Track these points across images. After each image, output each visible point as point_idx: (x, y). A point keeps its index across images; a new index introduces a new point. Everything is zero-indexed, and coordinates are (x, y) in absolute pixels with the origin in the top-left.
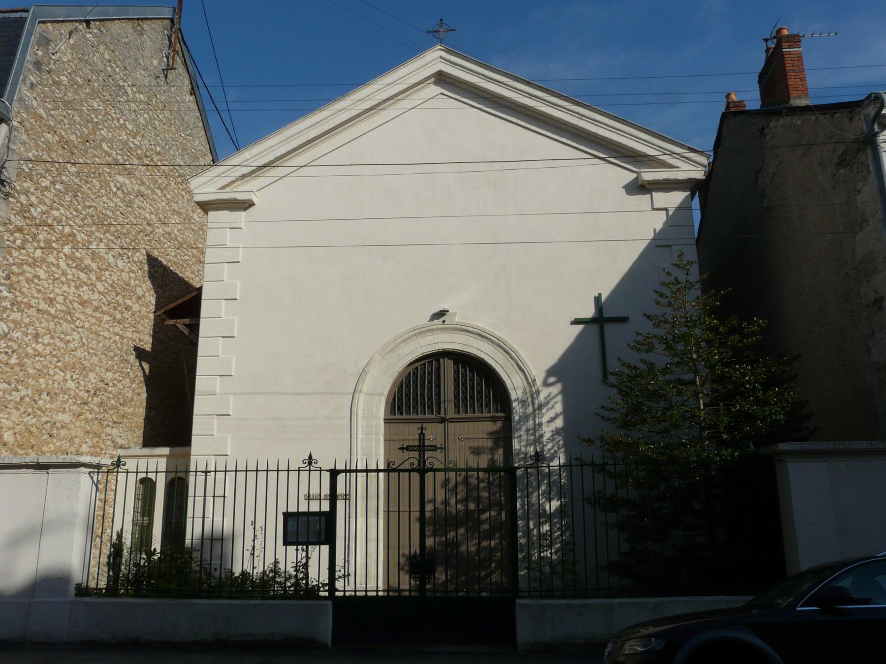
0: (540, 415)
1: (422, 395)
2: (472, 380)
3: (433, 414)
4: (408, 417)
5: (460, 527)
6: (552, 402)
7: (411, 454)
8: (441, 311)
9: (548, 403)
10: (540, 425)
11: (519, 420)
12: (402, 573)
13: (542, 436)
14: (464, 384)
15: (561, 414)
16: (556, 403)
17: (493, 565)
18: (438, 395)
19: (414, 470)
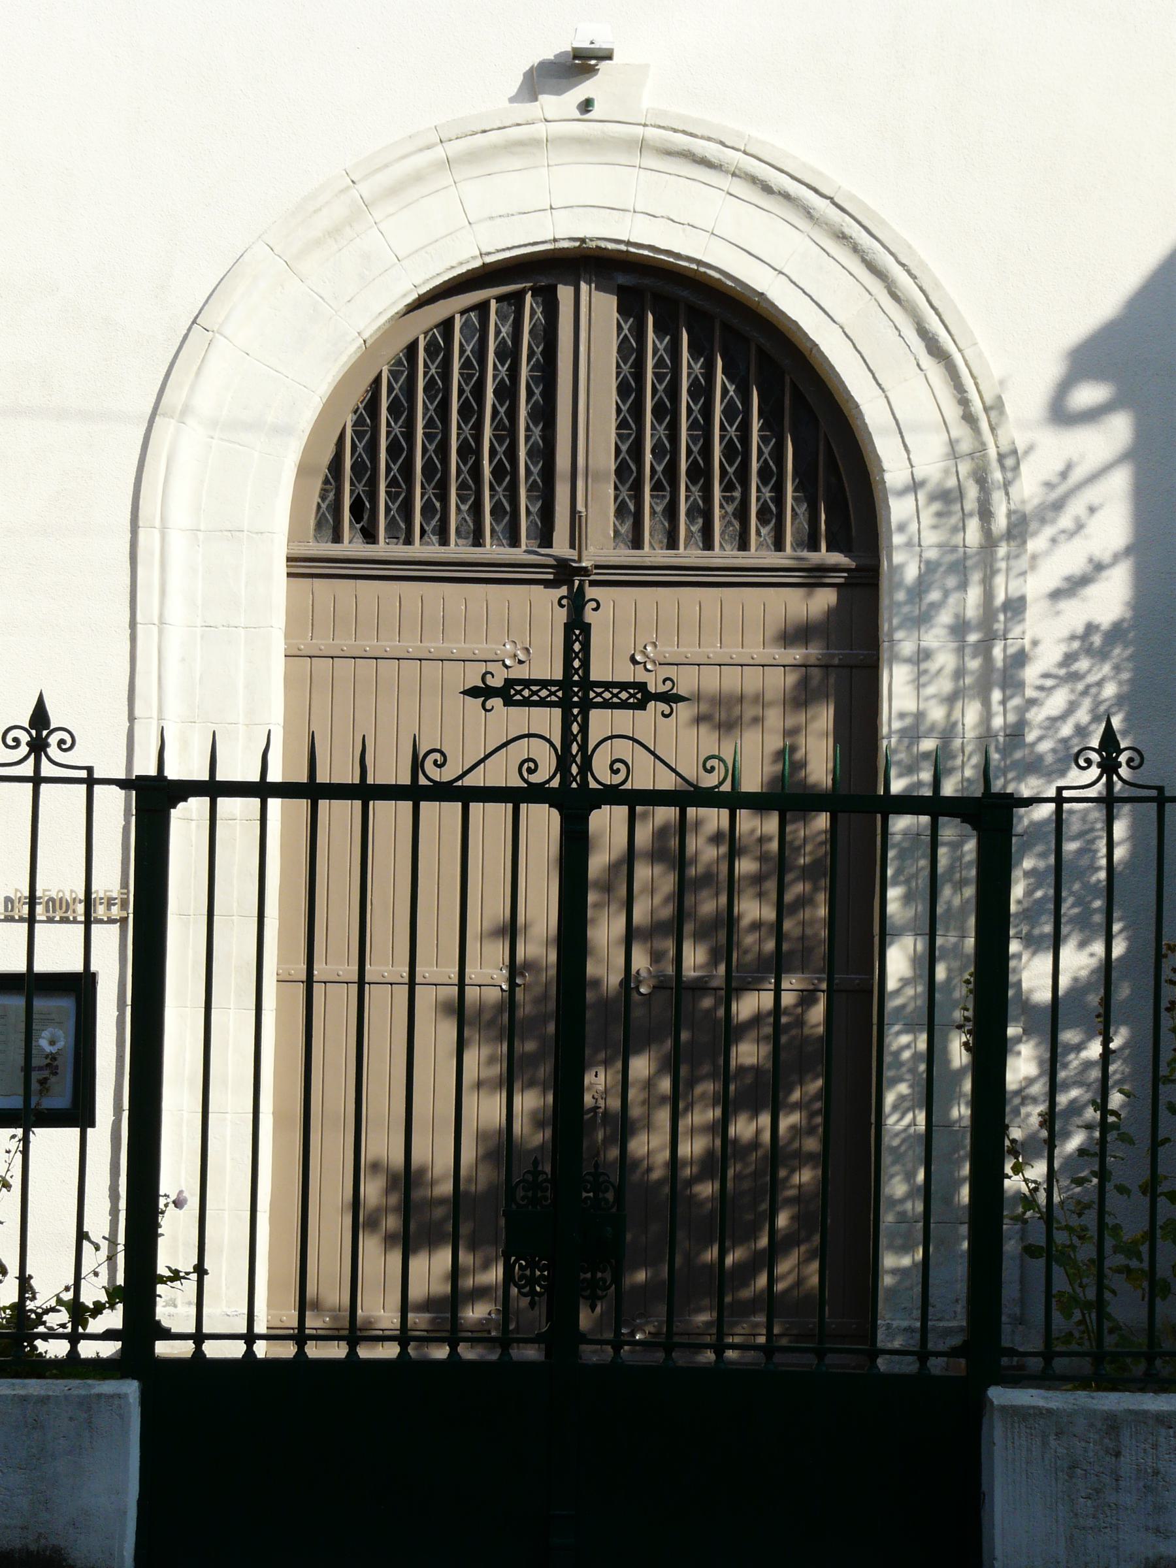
0: (1023, 563)
1: (470, 451)
2: (702, 391)
3: (514, 542)
4: (399, 551)
5: (638, 1052)
6: (1076, 508)
7: (519, 719)
8: (578, 54)
9: (1058, 506)
10: (1016, 607)
11: (921, 579)
12: (370, 1245)
13: (1020, 659)
14: (666, 411)
15: (1116, 558)
16: (1092, 510)
17: (782, 1220)
18: (545, 453)
19: (535, 793)
